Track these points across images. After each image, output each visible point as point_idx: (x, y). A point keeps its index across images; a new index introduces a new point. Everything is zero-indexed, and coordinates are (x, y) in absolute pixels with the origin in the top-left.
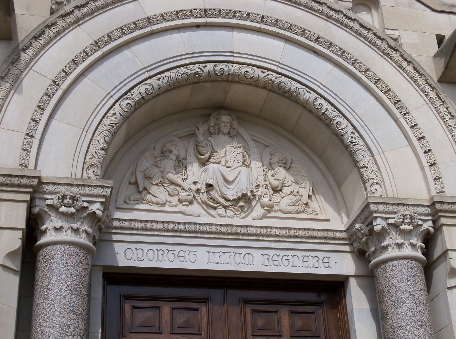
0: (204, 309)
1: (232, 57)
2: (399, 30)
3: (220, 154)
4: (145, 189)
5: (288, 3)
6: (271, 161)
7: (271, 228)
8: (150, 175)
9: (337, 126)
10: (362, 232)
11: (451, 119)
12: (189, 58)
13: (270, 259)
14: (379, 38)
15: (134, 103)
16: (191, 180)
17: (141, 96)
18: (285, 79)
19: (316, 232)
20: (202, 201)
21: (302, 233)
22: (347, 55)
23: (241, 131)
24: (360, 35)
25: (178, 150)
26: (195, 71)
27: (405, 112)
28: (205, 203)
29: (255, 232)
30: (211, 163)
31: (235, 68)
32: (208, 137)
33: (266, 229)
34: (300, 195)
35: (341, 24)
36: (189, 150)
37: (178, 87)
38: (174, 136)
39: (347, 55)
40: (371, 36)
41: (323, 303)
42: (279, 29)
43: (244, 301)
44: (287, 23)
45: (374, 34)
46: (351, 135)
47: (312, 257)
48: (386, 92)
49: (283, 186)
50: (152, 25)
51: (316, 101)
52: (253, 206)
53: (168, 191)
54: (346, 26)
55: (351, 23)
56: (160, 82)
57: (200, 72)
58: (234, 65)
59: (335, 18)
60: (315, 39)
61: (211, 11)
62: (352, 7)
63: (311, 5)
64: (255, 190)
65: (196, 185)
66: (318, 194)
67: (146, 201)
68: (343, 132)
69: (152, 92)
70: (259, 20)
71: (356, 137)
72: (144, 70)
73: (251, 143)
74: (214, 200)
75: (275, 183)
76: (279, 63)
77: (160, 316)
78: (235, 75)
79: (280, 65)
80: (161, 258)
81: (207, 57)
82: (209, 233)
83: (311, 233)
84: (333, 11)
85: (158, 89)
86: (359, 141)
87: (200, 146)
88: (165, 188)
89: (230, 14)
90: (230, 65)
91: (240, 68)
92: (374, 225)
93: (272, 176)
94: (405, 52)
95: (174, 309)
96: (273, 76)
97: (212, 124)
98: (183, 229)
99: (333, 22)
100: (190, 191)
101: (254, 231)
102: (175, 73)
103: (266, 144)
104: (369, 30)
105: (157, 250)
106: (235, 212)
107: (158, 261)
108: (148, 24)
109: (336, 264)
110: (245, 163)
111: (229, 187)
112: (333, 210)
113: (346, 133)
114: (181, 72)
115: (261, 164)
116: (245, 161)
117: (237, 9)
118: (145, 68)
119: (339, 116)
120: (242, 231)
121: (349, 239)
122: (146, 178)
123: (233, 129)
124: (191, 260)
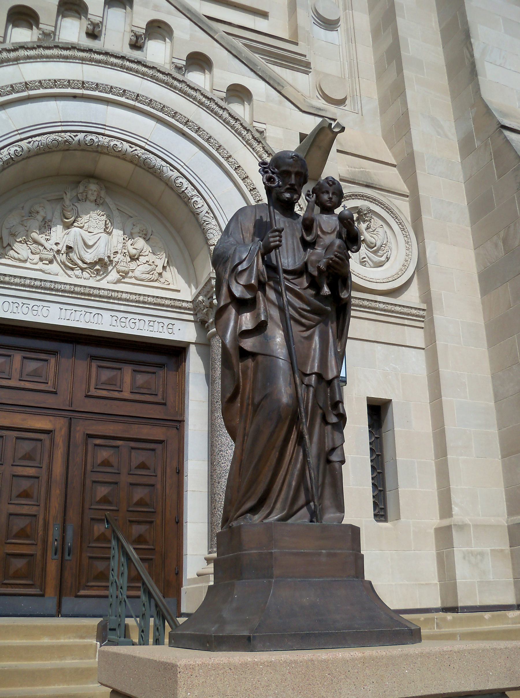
0: (53, 361)
1: (104, 130)
2: (266, 124)
3: (84, 219)
4: (9, 245)
5: (164, 86)
6: (132, 231)
7: (122, 292)
8: (15, 232)
9: (194, 205)
10: (204, 304)
11: (300, 210)
12: (61, 125)
13: (118, 321)
14: (245, 128)
15: (2, 163)
16: (53, 241)
17: (10, 157)
18: (151, 156)
19: (164, 300)
20: (61, 261)
21: (150, 299)
22: (212, 141)
23: (108, 200)
24: (228, 123)
25: (46, 212)
26: (65, 139)
27: (258, 199)
28: (64, 263)
29: (106, 294)
30: (75, 226)
31: (105, 141)
32: (76, 203)
33: (117, 293)
34: (155, 265)
35: (212, 111)
36: (56, 213)
37: (49, 152)
38: (43, 198)
39: (212, 141)
40: (238, 126)
41: (164, 365)
42: (153, 109)
43: (91, 357)
44: (160, 104)
45: (241, 124)
46: (206, 215)
47: (158, 322)
48: (243, 179)
49: (140, 255)
50: (29, 90)
51: (178, 179)
52: (109, 270)
53: (31, 250)
54: (216, 113)
55: (221, 112)
56: (30, 145)
57: (70, 140)
58: (104, 137)
59: (207, 105)
60: (185, 122)
61: (89, 83)
62: (225, 97)
63: (185, 90)
64: (112, 256)
65: (57, 246)
66: (172, 266)
67: (9, 256)
68: (199, 211)
69: (21, 154)
70: (134, 97)
71: (210, 217)
72: (16, 133)
73: (116, 213)
74: (72, 261)
75: (133, 252)
76: (148, 140)
77: (11, 363)
78: (104, 146)
79: (148, 143)
80: (15, 310)
81: (79, 127)
82: (63, 291)
83: (159, 301)
84: (205, 98)
85: (27, 152)
86: (212, 220)
87: (65, 210)
88: (28, 246)
89: (107, 89)
90: (100, 136)
91: (109, 141)
92: (214, 298)
93: (131, 245)
94: (267, 144)
95: (25, 358)
96: (140, 152)
97: (81, 191)
98: (39, 286)
99: (204, 108)
100: (51, 251)
101: (106, 293)
102: (46, 138)
103: (130, 215)
104: (237, 120)
105: (12, 302)
106: (91, 274)
107: (12, 313)
108: (25, 89)
109: (180, 331)
110: (107, 230)
111: (89, 251)
112: (184, 282)
113: (201, 212)
114: (52, 138)
115: (122, 232)
116: (107, 228)
117: (114, 85)
118: (17, 130)
119: (197, 196)
120: (95, 293)
121: (194, 309)
122: (11, 234)
123: (101, 197)
124: (327, 92)
